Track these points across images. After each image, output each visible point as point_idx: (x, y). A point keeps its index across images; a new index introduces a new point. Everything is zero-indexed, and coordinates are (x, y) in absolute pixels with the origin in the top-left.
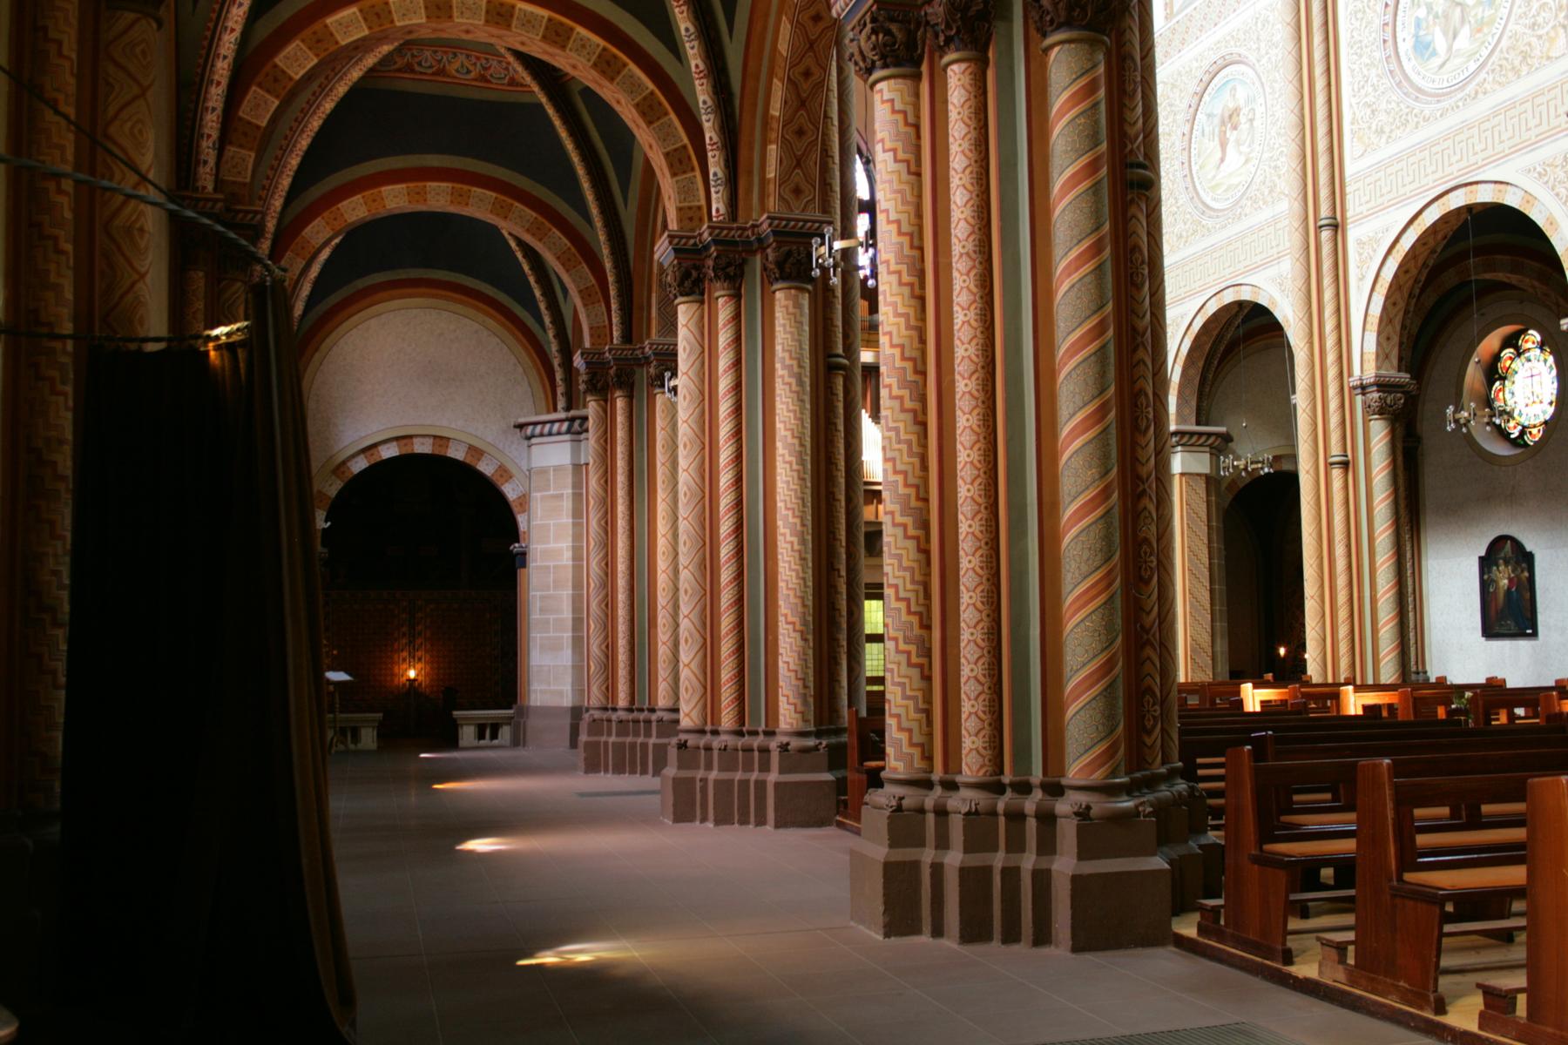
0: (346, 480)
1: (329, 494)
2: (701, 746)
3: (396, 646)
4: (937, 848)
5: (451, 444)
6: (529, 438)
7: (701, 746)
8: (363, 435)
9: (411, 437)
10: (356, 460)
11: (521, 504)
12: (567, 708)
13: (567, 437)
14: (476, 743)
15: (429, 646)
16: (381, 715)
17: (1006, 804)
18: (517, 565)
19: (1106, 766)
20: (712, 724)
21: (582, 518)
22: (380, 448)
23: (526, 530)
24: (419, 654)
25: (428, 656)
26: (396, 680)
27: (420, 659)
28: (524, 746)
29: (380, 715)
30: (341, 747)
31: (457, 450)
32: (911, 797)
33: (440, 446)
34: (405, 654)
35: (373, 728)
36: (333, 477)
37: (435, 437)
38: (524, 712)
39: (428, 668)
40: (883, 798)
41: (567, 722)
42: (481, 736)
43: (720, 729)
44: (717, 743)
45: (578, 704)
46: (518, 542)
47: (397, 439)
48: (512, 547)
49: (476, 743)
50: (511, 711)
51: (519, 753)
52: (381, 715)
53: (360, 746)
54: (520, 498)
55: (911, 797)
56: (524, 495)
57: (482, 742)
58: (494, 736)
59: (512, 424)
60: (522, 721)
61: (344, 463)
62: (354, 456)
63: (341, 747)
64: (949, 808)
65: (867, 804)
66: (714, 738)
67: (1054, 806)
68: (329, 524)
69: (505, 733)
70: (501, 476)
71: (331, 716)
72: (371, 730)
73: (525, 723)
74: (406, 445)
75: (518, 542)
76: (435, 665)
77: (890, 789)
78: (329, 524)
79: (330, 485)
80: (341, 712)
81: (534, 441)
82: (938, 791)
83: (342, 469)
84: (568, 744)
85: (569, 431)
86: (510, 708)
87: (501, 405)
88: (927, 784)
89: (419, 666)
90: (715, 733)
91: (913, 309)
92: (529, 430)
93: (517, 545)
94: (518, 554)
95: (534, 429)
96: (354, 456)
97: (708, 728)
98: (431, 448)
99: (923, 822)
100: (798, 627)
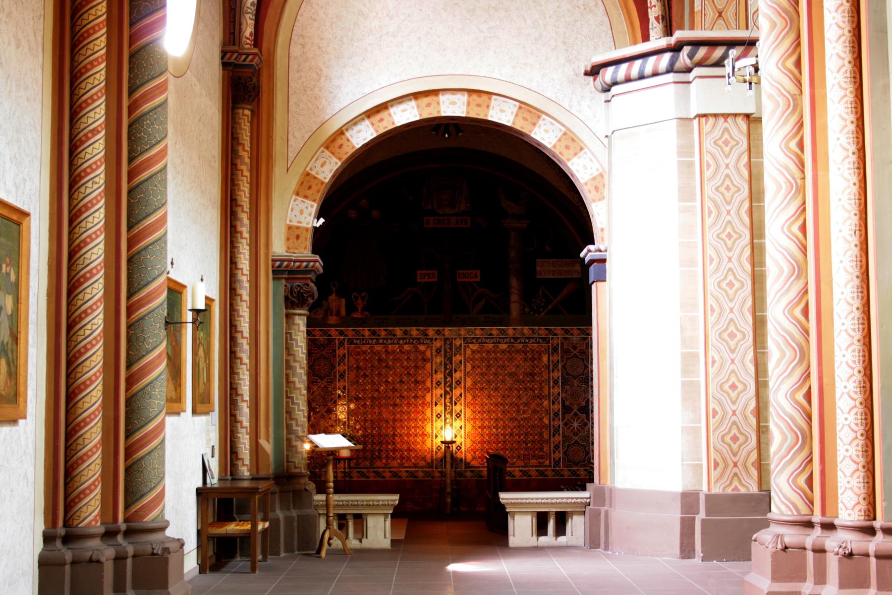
0: (345, 157)
1: (321, 177)
2: (872, 553)
3: (428, 398)
4: (815, 584)
5: (493, 103)
6: (607, 89)
7: (872, 553)
8: (367, 91)
9: (435, 92)
10: (356, 128)
11: (597, 188)
12: (675, 493)
13: (671, 77)
14: (533, 541)
15: (469, 398)
16: (396, 497)
17: (877, 545)
18: (591, 280)
19: (133, 371)
20: (823, 513)
21: (694, 200)
22: (392, 110)
23: (605, 226)
24: (457, 408)
25: (469, 412)
26: (428, 444)
27: (458, 416)
28: (606, 548)
29: (395, 498)
30: (337, 543)
31: (502, 111)
32: (791, 536)
33: (479, 105)
34: (440, 408)
35: (386, 515)
36: (327, 153)
37: (471, 92)
38: (602, 496)
39: (469, 427)
40: (766, 536)
41: (675, 516)
42: (541, 529)
43: (837, 522)
44: (833, 542)
45: (690, 488)
46: (593, 243)
47: (416, 96)
48: (582, 255)
49: (533, 541)
50: (585, 494)
51: (562, 540)
52: (396, 497)
53: (367, 543)
54: (594, 179)
55: (791, 536)
56: (601, 175)
57: (543, 539)
58: (561, 530)
59: (583, 71)
60: (603, 509)
61: (341, 132)
62: (355, 122)
63: (337, 543)
64: (827, 548)
65: (755, 540)
66: (827, 533)
67: (883, 538)
68: (322, 220)
69: (577, 526)
70: (567, 147)
71: (322, 497)
72: (382, 519)
73: (607, 513)
74: (428, 105)
75: (593, 243)
76: (478, 423)
77: (775, 529)
78: (322, 220)
79: (323, 165)
80: (337, 491)
81: (615, 90)
82: (818, 531)
83: (339, 141)
84: (677, 551)
85: (670, 70)
86: (584, 489)
87: (565, 43)
88: (809, 525)
89: (458, 423)
90: (829, 527)
91: (239, 431)
92: (608, 74)
93: (591, 247)
94: (592, 261)
95: (629, 68)
96: (355, 122)
97: (817, 518)
98: (464, 108)
99: (805, 557)
100: (239, 398)
